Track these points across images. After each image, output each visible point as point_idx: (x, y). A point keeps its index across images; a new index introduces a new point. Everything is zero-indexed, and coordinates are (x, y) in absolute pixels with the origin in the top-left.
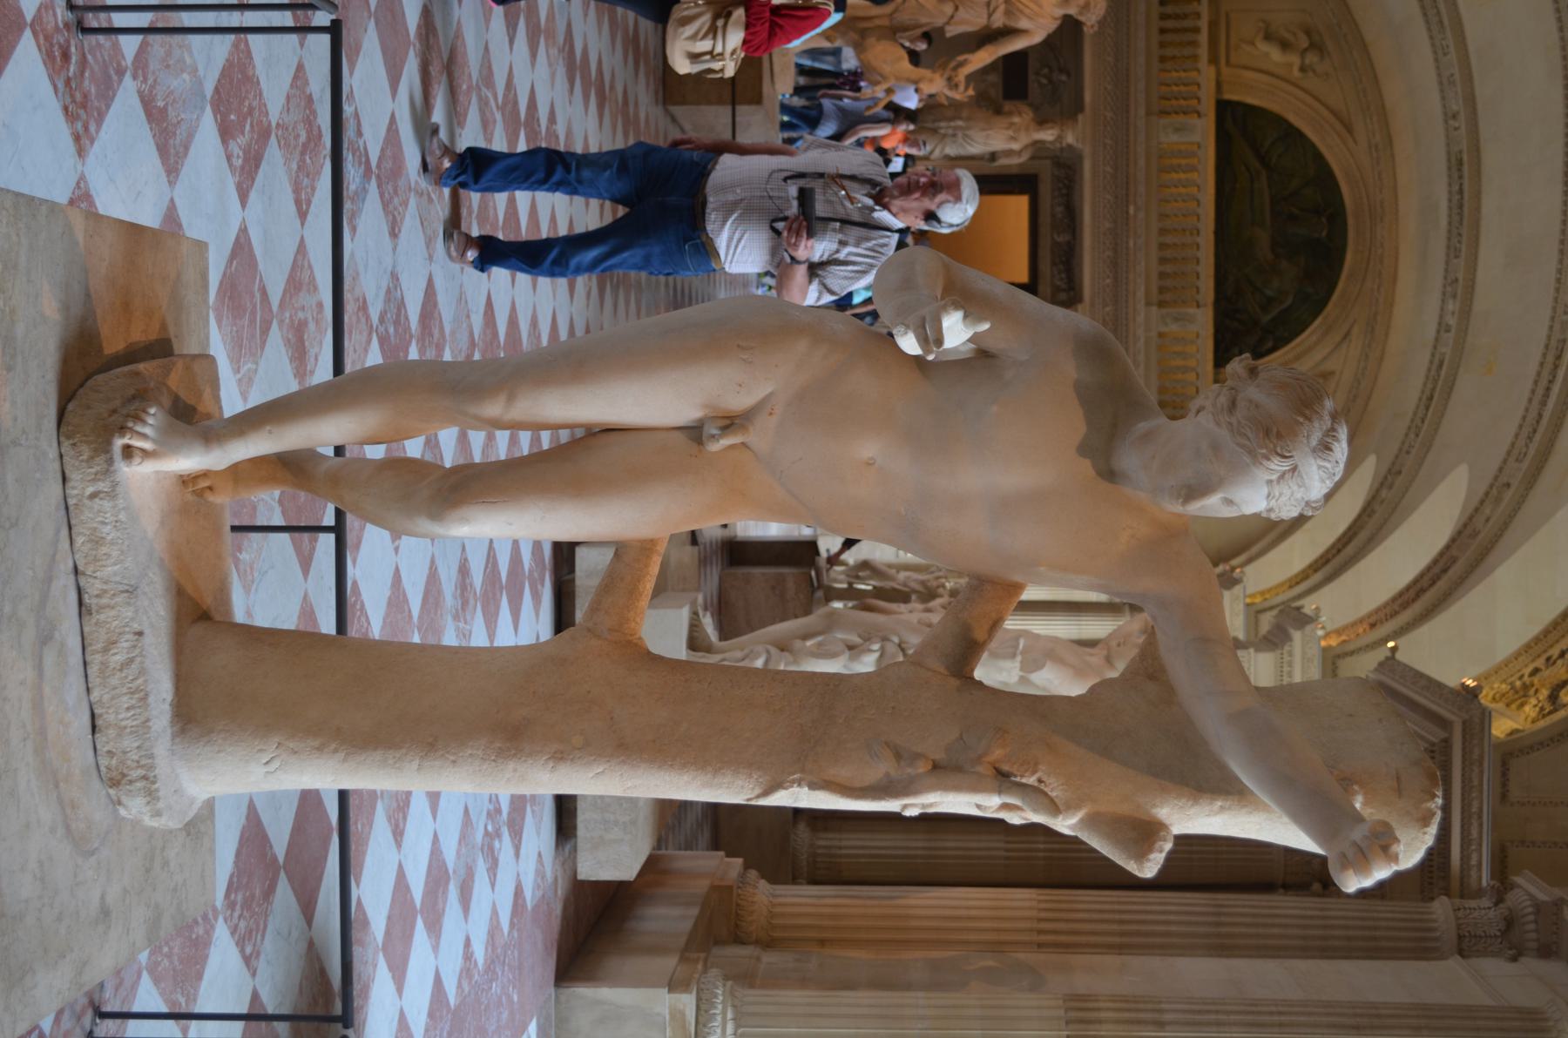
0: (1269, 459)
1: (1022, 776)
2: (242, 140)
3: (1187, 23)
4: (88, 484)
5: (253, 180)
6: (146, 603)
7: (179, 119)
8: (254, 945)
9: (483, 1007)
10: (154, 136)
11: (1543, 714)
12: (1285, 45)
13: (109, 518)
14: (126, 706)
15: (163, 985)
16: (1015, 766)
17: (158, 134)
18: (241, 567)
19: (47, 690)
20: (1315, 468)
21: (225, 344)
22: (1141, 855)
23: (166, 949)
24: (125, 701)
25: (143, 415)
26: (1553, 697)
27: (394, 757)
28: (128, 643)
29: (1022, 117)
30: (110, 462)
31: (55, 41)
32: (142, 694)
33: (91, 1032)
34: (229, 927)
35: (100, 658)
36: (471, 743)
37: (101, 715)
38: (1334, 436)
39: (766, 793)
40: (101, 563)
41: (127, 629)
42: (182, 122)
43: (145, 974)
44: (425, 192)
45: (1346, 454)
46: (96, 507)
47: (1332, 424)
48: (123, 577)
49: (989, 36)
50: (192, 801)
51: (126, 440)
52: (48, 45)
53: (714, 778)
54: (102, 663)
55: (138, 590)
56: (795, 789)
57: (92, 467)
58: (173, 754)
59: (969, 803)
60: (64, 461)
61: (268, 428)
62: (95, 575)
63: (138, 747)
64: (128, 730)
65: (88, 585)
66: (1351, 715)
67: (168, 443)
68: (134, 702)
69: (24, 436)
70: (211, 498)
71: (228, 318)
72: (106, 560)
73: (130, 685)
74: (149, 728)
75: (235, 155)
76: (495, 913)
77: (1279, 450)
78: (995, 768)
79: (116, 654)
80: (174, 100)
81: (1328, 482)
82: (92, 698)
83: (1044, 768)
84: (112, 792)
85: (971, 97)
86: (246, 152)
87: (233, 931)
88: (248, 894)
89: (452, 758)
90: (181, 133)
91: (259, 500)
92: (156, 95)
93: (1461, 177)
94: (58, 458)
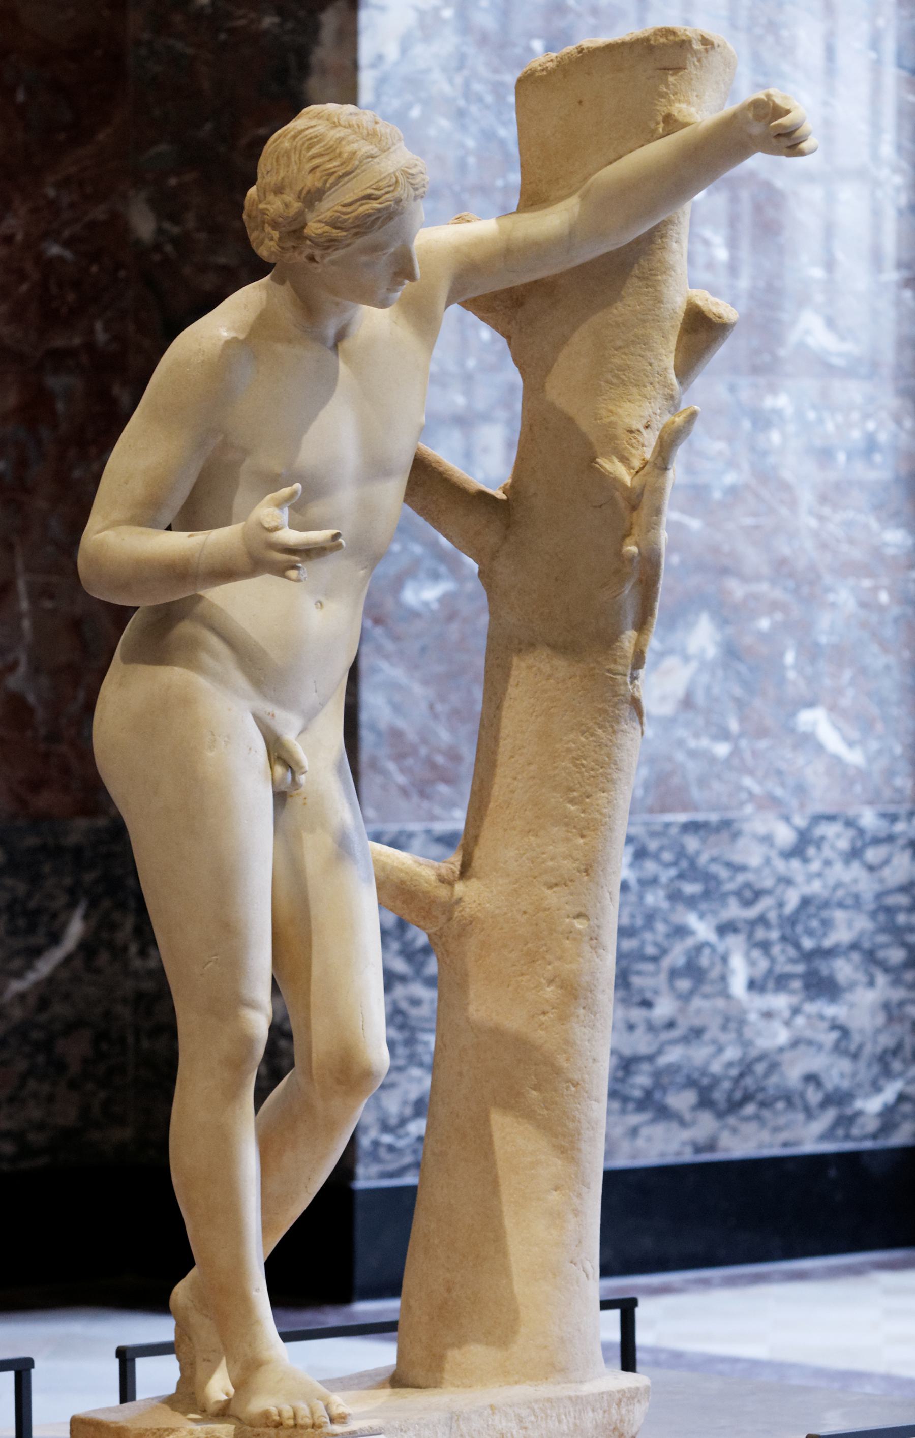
14: (557, 1424)
61: (254, 1293)
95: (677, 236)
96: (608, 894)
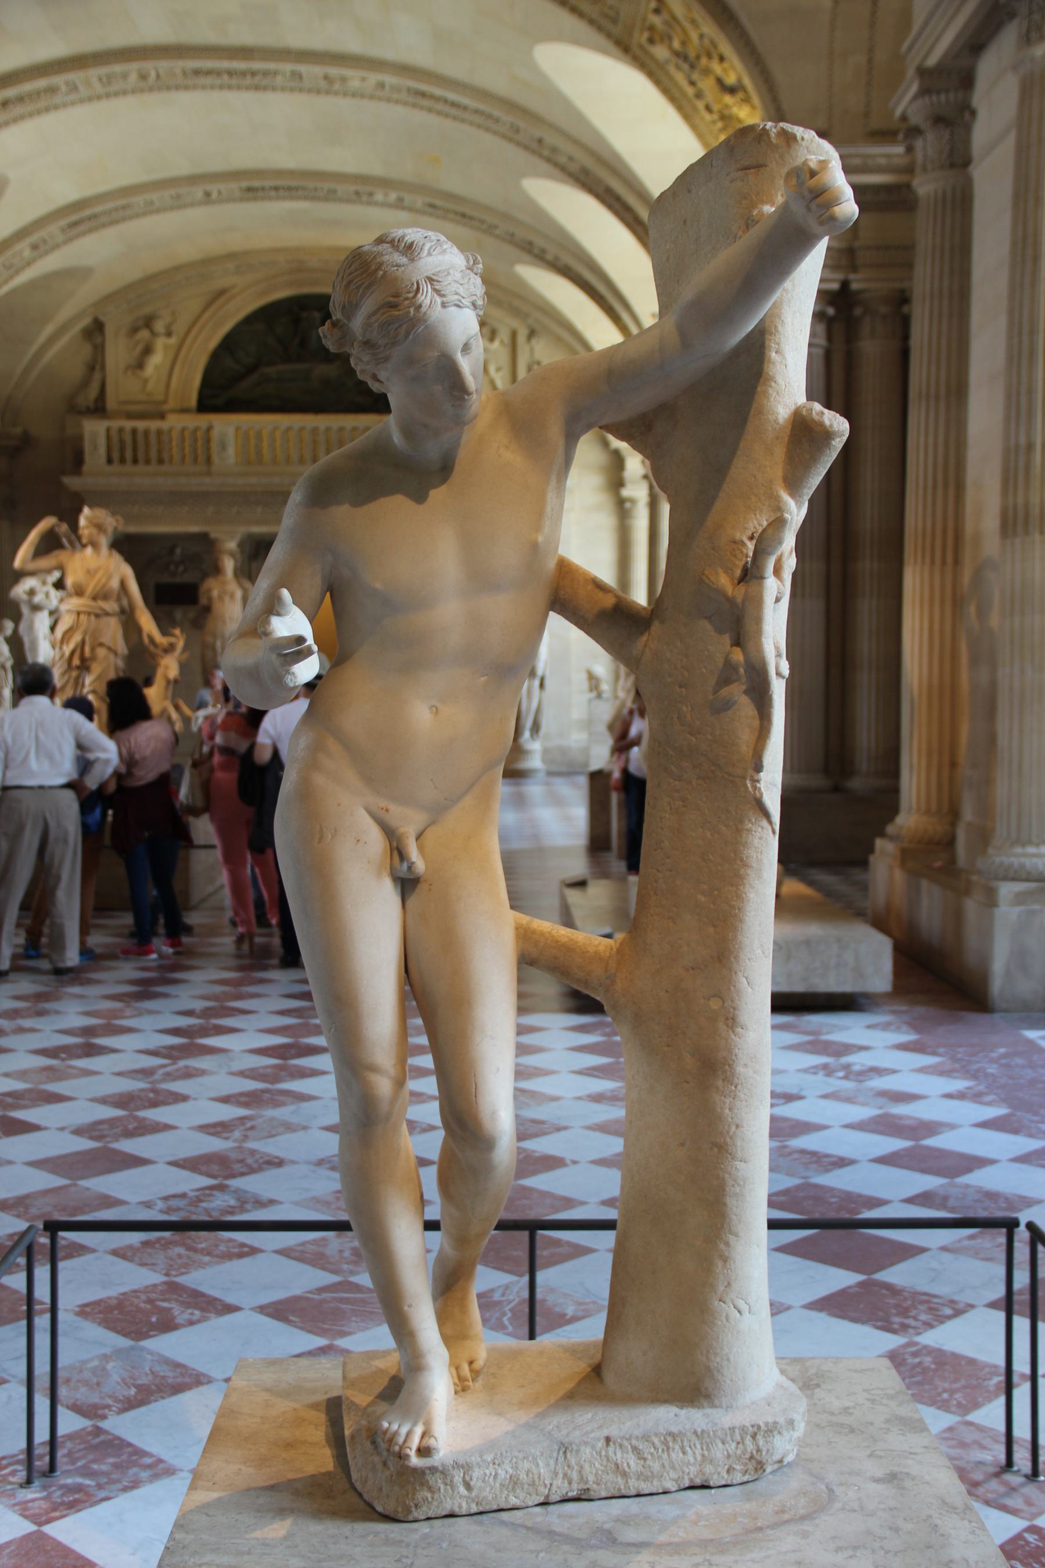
0: (420, 306)
1: (747, 556)
2: (176, 1309)
3: (128, 438)
4: (456, 1493)
5: (216, 1299)
6: (577, 1433)
7: (149, 1372)
8: (943, 1305)
9: (1011, 1082)
10: (163, 1398)
11: (747, 100)
12: (148, 351)
13: (491, 1470)
14: (681, 1455)
15: (980, 1399)
16: (737, 562)
17: (162, 1394)
18: (580, 1314)
19: (662, 1538)
20: (430, 259)
21: (367, 1328)
22: (827, 435)
23: (945, 1396)
24: (676, 1455)
25: (388, 1436)
26: (732, 90)
27: (733, 1186)
28: (617, 1453)
29: (212, 587)
30: (433, 1469)
31: (59, 1500)
32: (669, 1439)
33: (1026, 1476)
34: (925, 1331)
35: (633, 1480)
36: (719, 1110)
37: (691, 1480)
38: (399, 241)
39: (767, 815)
40: (537, 1480)
41: (603, 1453)
42: (153, 1370)
43: (970, 1418)
44: (244, 1133)
45: (419, 230)
46: (480, 1484)
47: (387, 243)
48: (550, 1457)
49: (128, 617)
50: (779, 1386)
51: (412, 1453)
52: (61, 1508)
53: (751, 867)
54: (638, 1479)
55: (564, 1441)
56: (762, 785)
57: (439, 1488)
58: (732, 1407)
59: (775, 610)
60: (433, 1516)
61: (406, 1308)
62: (549, 1486)
63: (723, 1443)
64: (706, 1453)
65: (558, 1492)
66: (685, 222)
67: (418, 1410)
68: (677, 1447)
69: (404, 1560)
70: (480, 1363)
71: (343, 1325)
72: (533, 1474)
73: (660, 1450)
74: (703, 1431)
75: (191, 1316)
76: (923, 1070)
77: (411, 295)
78: (739, 583)
79: (628, 1464)
80: (131, 1377)
81: (445, 247)
82: (674, 1489)
83: (738, 534)
84: (769, 1469)
85: (182, 632)
86: (187, 1305)
87: (929, 1326)
88: (894, 1311)
89: (733, 1128)
90: (164, 1371)
91: (519, 1297)
92: (123, 1396)
93: (263, 189)
94: (431, 1522)
95: (777, 346)
96: (745, 979)
